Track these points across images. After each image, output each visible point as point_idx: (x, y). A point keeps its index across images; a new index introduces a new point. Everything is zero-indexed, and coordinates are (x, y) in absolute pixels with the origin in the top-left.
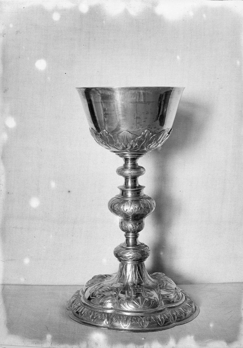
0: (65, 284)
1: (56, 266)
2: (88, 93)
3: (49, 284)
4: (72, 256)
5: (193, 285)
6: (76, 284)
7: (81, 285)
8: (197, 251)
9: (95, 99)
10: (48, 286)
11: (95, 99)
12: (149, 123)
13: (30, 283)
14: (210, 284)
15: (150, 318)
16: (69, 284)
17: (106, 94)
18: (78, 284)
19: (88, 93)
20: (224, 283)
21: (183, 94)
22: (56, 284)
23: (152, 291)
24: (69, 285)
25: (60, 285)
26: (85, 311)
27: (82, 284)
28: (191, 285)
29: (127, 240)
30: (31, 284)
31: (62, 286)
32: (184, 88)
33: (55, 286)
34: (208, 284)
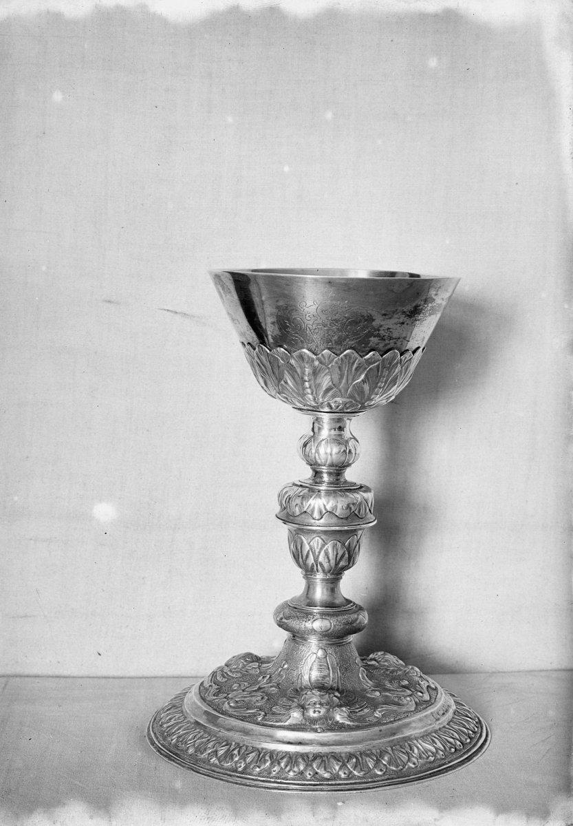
0: (152, 675)
1: (132, 629)
2: (242, 287)
3: (116, 675)
4: (169, 608)
5: (457, 675)
6: (179, 673)
7: (190, 675)
8: (477, 600)
9: (257, 300)
10: (112, 680)
11: (257, 300)
12: (379, 340)
13: (66, 673)
14: (499, 672)
15: (321, 687)
16: (162, 673)
17: (282, 284)
18: (184, 674)
19: (242, 287)
20: (531, 671)
21: (457, 288)
22: (132, 674)
23: (374, 660)
24: (162, 677)
25: (141, 675)
26: (209, 733)
27: (193, 672)
28: (453, 675)
29: (309, 588)
30: (72, 675)
31: (145, 678)
32: (459, 280)
33: (129, 678)
34: (494, 672)
